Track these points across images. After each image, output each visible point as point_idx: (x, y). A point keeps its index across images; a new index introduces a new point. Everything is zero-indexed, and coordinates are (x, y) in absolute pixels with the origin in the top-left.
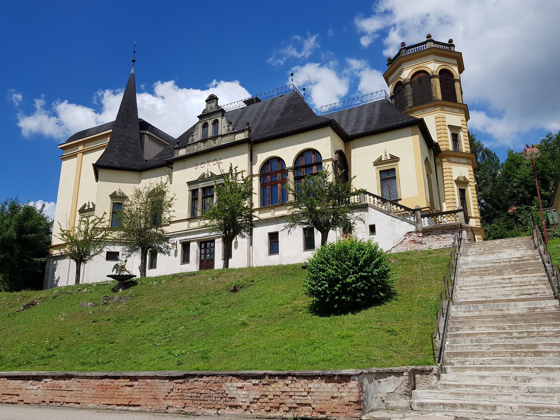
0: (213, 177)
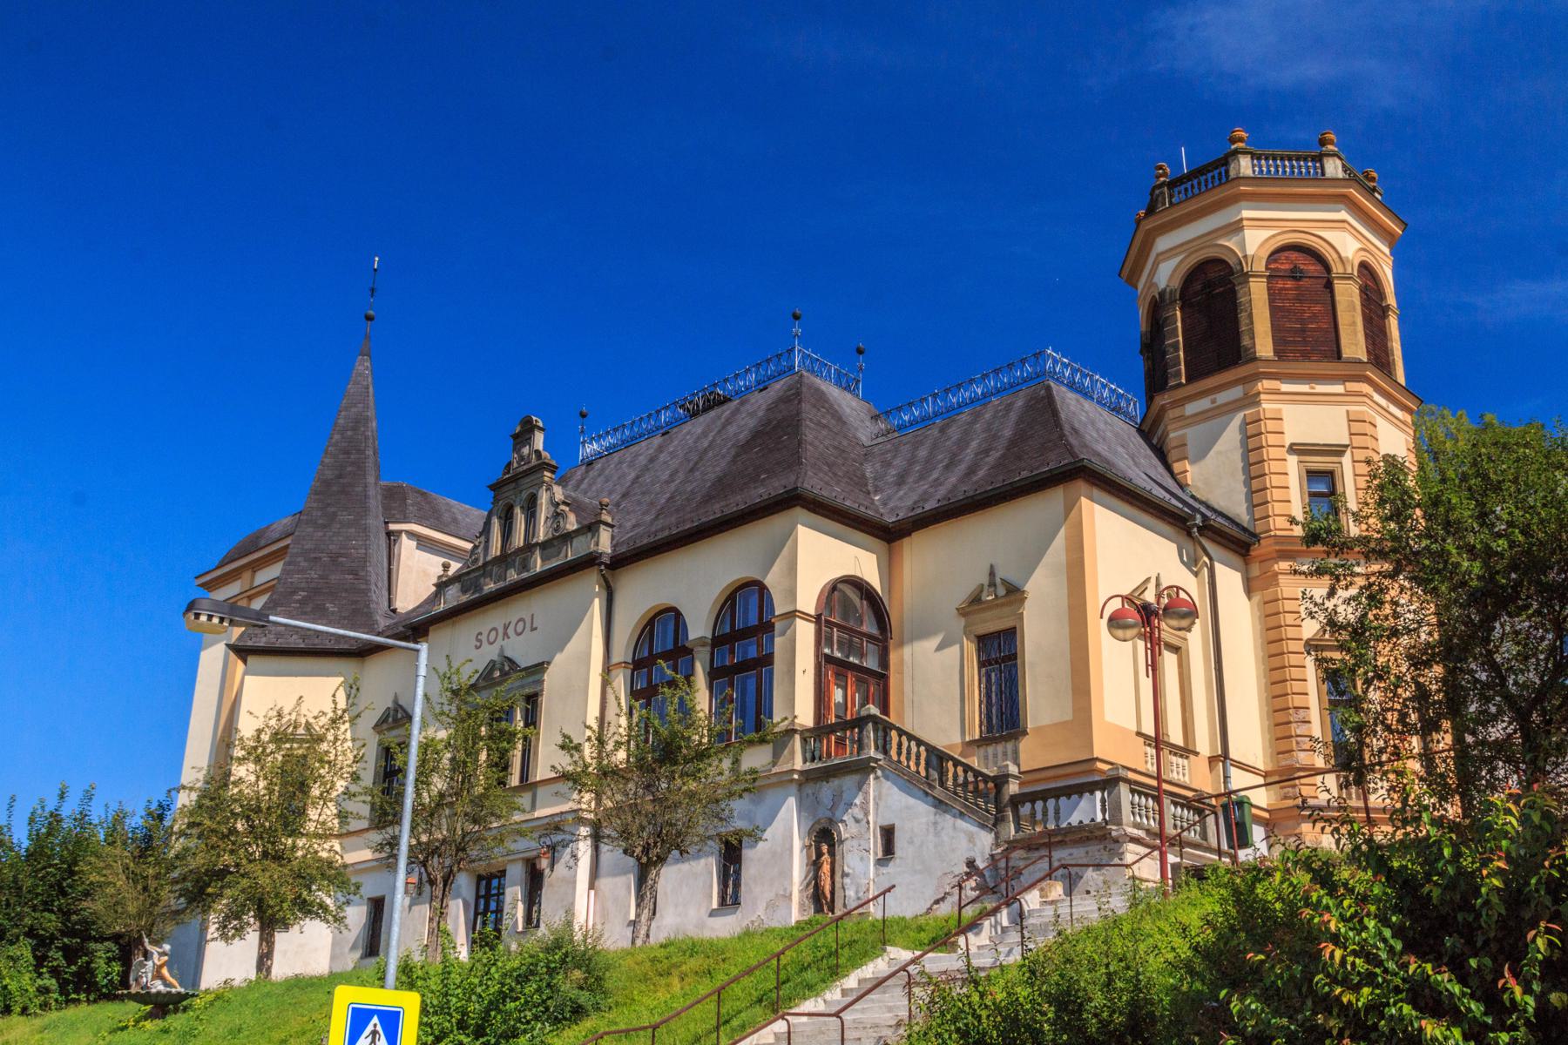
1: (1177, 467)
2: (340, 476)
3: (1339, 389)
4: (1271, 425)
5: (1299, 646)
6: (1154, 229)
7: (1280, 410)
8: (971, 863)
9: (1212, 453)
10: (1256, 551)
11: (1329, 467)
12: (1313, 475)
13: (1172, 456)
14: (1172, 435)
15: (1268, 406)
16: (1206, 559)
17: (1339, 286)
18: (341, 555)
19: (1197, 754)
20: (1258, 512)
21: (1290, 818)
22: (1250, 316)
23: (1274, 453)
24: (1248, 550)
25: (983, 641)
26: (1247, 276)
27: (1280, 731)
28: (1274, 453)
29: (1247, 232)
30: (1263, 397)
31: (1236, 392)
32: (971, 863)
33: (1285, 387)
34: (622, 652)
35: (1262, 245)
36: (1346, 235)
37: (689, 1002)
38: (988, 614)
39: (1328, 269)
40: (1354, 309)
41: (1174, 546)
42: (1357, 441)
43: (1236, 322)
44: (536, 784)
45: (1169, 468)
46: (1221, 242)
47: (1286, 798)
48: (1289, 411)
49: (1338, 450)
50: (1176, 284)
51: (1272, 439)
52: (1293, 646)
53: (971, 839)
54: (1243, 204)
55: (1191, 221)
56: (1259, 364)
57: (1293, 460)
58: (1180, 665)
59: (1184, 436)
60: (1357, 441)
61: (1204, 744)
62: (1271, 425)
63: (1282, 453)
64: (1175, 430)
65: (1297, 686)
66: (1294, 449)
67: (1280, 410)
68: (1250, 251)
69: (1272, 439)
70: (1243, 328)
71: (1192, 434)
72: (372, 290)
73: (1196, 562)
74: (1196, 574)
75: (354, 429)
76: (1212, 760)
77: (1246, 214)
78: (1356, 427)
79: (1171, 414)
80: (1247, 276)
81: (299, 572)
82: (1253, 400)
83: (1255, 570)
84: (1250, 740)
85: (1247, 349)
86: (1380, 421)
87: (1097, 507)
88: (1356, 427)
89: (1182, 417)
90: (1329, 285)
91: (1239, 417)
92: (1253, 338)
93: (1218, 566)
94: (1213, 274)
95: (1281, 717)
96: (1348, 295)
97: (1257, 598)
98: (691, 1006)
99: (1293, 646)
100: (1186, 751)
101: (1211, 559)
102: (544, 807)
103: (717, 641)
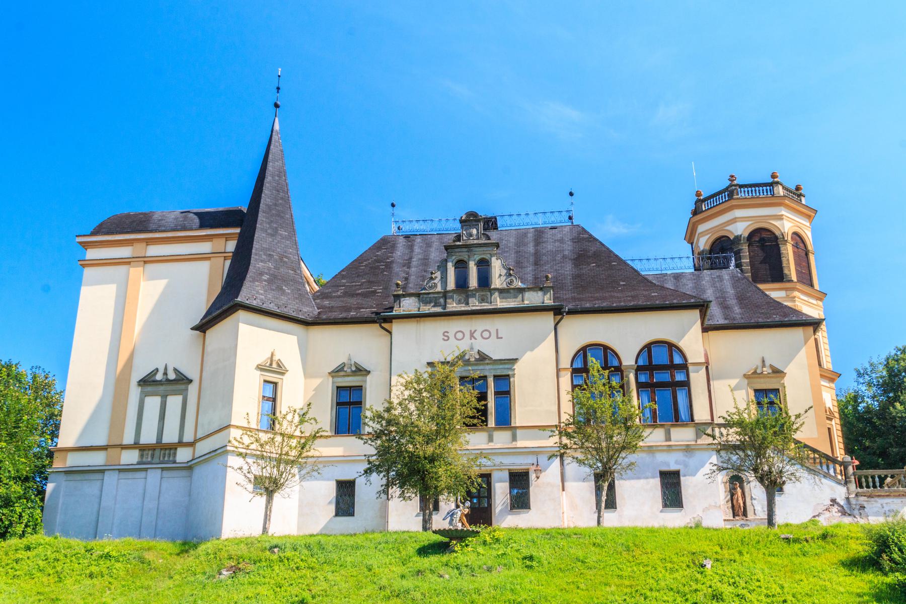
0: (483, 358)
2: (276, 205)
8: (834, 501)
18: (286, 257)
25: (760, 393)
32: (834, 501)
34: (566, 362)
38: (762, 380)
43: (780, 262)
44: (516, 428)
53: (832, 489)
70: (784, 265)
72: (278, 88)
75: (279, 176)
77: (783, 213)
81: (262, 261)
87: (236, 242)
94: (764, 235)
96: (788, 252)
102: (523, 439)
103: (639, 369)
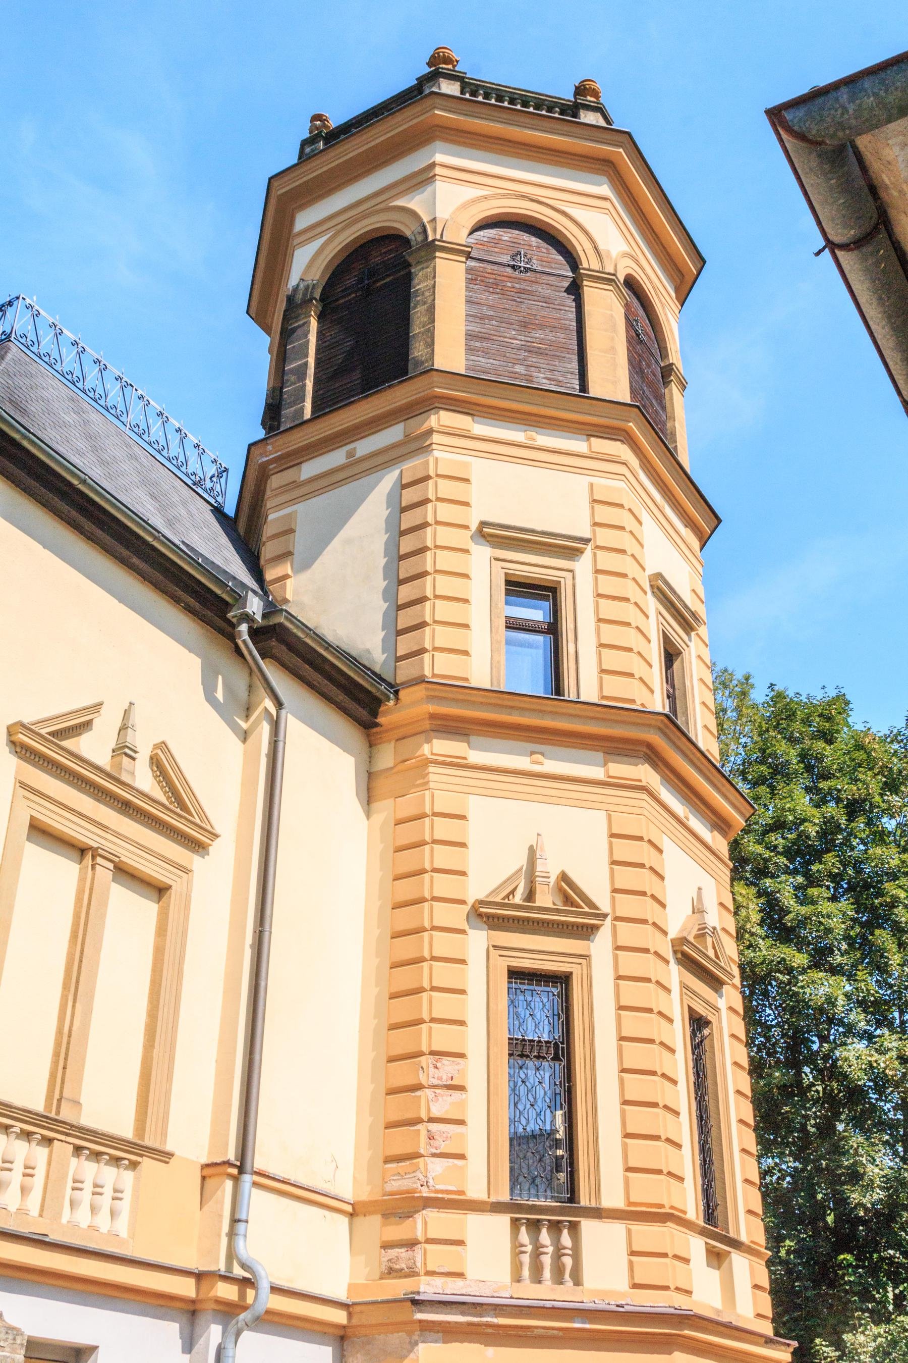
1: (270, 574)
3: (579, 445)
4: (446, 488)
5: (456, 916)
6: (296, 208)
7: (467, 465)
9: (336, 542)
10: (391, 715)
11: (549, 575)
12: (518, 588)
13: (268, 551)
14: (271, 517)
15: (443, 456)
16: (269, 704)
17: (592, 293)
19: (165, 1156)
20: (405, 645)
21: (396, 1326)
22: (431, 310)
23: (445, 536)
24: (375, 713)
26: (430, 248)
27: (399, 1108)
28: (445, 536)
29: (440, 186)
30: (436, 438)
31: (393, 434)
33: (480, 428)
35: (465, 206)
36: (607, 218)
37: (387, 1321)
39: (573, 261)
40: (614, 328)
41: (195, 663)
42: (604, 537)
45: (257, 573)
46: (400, 202)
47: (391, 1272)
48: (481, 470)
49: (569, 548)
50: (317, 275)
51: (445, 512)
52: (445, 915)
54: (438, 144)
55: (563, 731)
56: (435, 377)
57: (482, 554)
58: (161, 930)
59: (290, 516)
60: (604, 537)
61: (194, 1129)
62: (446, 488)
63: (461, 538)
64: (279, 507)
65: (443, 1005)
66: (493, 535)
67: (467, 465)
68: (443, 212)
69: (445, 512)
71: (306, 513)
73: (248, 711)
74: (245, 736)
76: (210, 1171)
77: (439, 158)
78: (605, 514)
79: (275, 481)
80: (430, 248)
82: (418, 445)
83: (386, 757)
84: (318, 1121)
85: (418, 363)
86: (645, 517)
88: (605, 514)
89: (295, 485)
90: (575, 290)
91: (388, 480)
92: (431, 345)
93: (293, 726)
95: (402, 1074)
97: (385, 809)
98: (387, 1324)
99: (445, 915)
100: (128, 1152)
101: (279, 705)
